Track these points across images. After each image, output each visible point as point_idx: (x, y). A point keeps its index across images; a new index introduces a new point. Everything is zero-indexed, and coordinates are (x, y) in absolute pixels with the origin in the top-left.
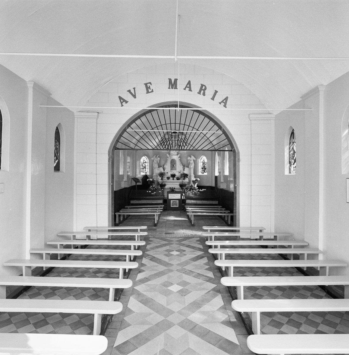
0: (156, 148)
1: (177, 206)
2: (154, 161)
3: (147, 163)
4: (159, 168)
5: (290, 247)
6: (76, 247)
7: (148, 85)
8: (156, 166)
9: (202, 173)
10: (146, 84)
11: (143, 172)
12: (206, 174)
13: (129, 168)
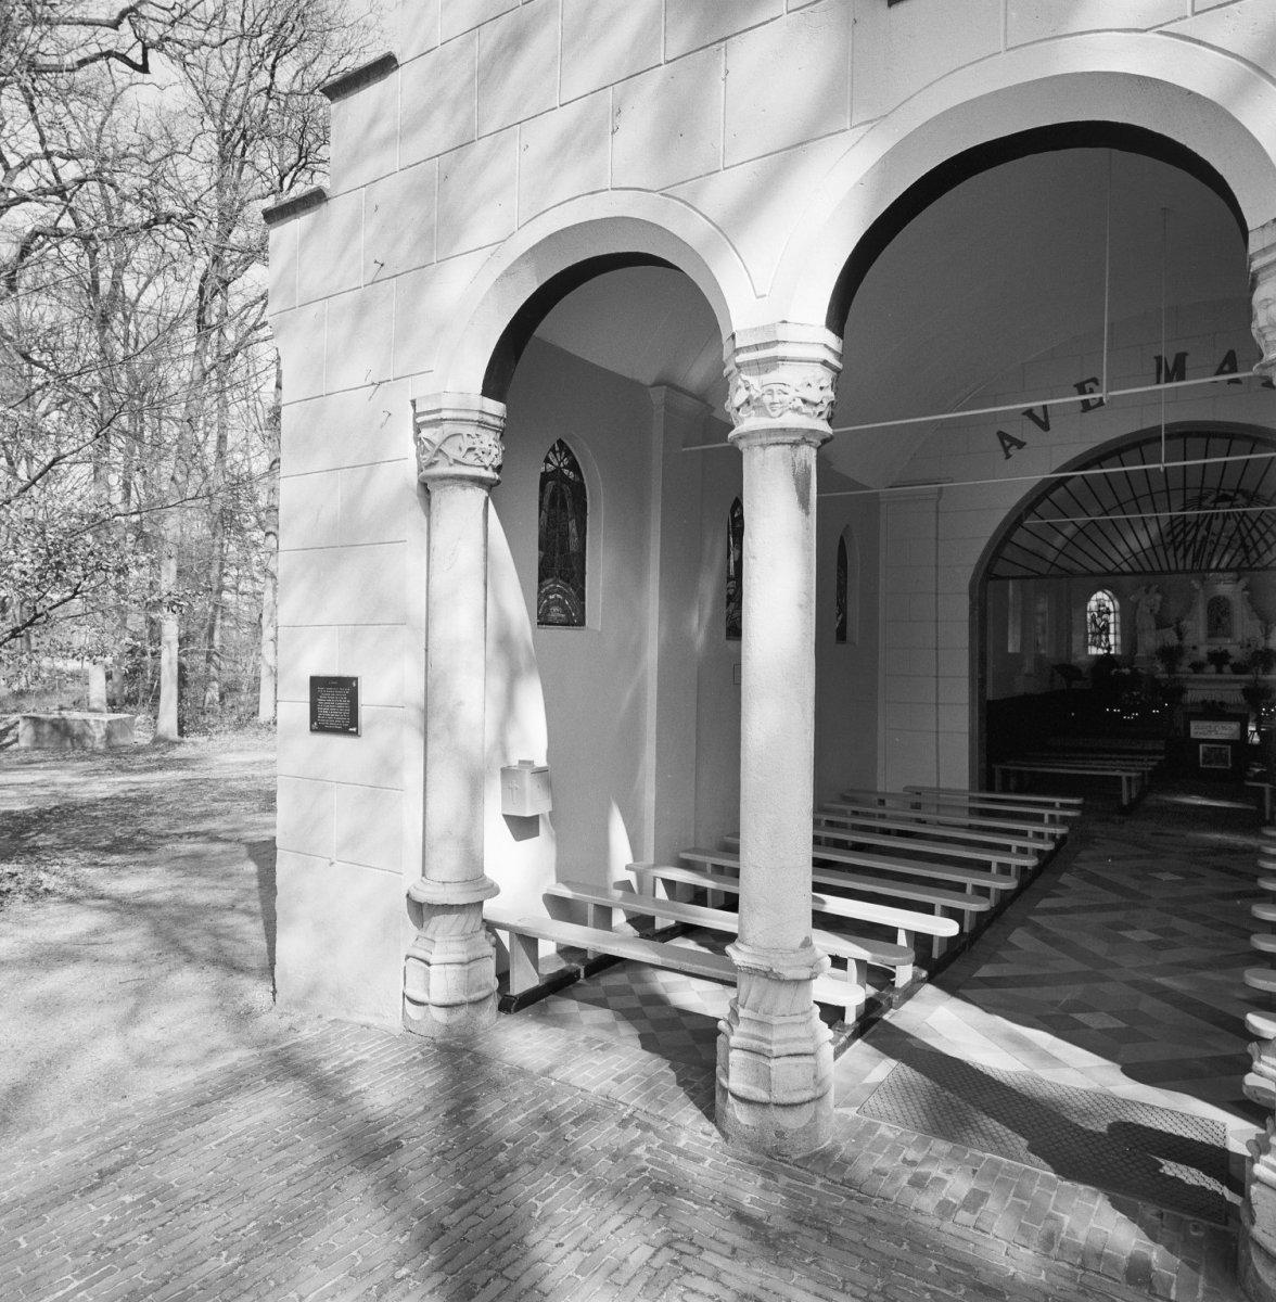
0: (1118, 570)
1: (1226, 762)
3: (1112, 616)
6: (886, 832)
8: (1147, 622)
11: (1099, 646)
13: (1044, 632)
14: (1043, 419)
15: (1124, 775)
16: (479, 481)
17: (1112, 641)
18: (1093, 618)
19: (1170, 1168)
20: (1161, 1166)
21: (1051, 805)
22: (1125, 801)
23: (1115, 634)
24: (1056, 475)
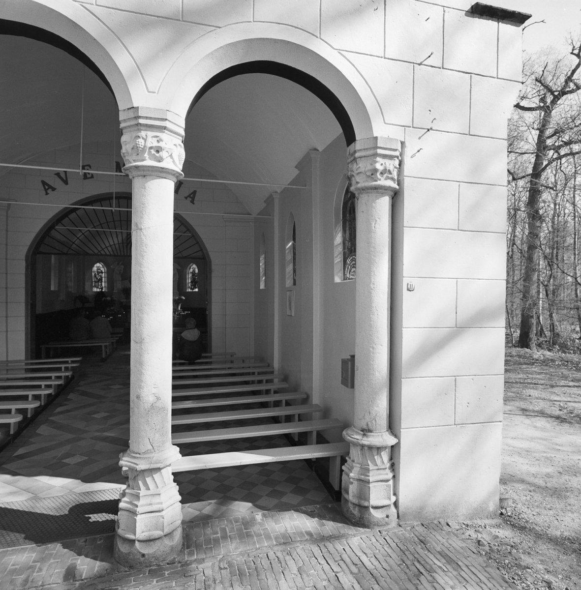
3: (104, 274)
9: (191, 289)
11: (97, 288)
12: (197, 290)
14: (65, 179)
15: (103, 345)
17: (103, 285)
18: (95, 275)
19: (95, 517)
20: (90, 518)
22: (104, 357)
23: (105, 282)
24: (71, 206)
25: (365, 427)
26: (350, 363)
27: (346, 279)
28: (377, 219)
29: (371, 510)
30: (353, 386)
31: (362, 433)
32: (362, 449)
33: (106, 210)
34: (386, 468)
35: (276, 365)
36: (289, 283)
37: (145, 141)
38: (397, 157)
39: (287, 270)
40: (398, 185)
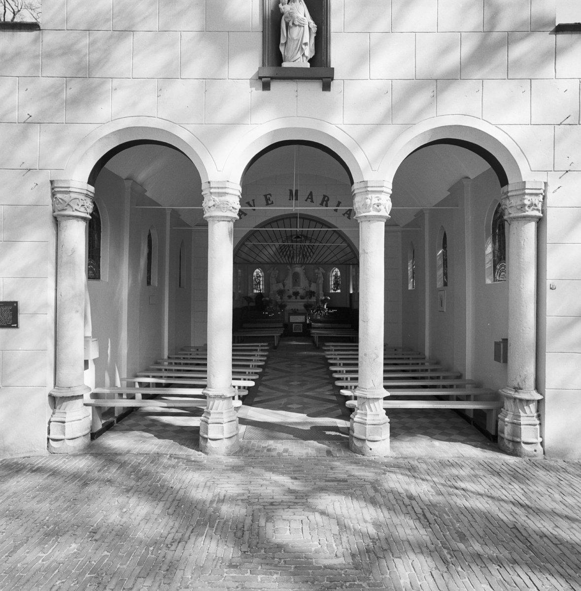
2: (271, 274)
4: (277, 284)
5: (438, 378)
7: (268, 196)
9: (334, 290)
10: (266, 196)
11: (257, 290)
12: (339, 291)
16: (84, 219)
19: (328, 433)
21: (258, 346)
25: (517, 386)
26: (502, 345)
27: (496, 281)
28: (526, 239)
29: (523, 444)
30: (506, 361)
31: (514, 390)
32: (514, 402)
33: (282, 230)
34: (534, 416)
35: (427, 353)
36: (440, 284)
37: (371, 201)
38: (542, 194)
39: (437, 273)
40: (542, 213)
